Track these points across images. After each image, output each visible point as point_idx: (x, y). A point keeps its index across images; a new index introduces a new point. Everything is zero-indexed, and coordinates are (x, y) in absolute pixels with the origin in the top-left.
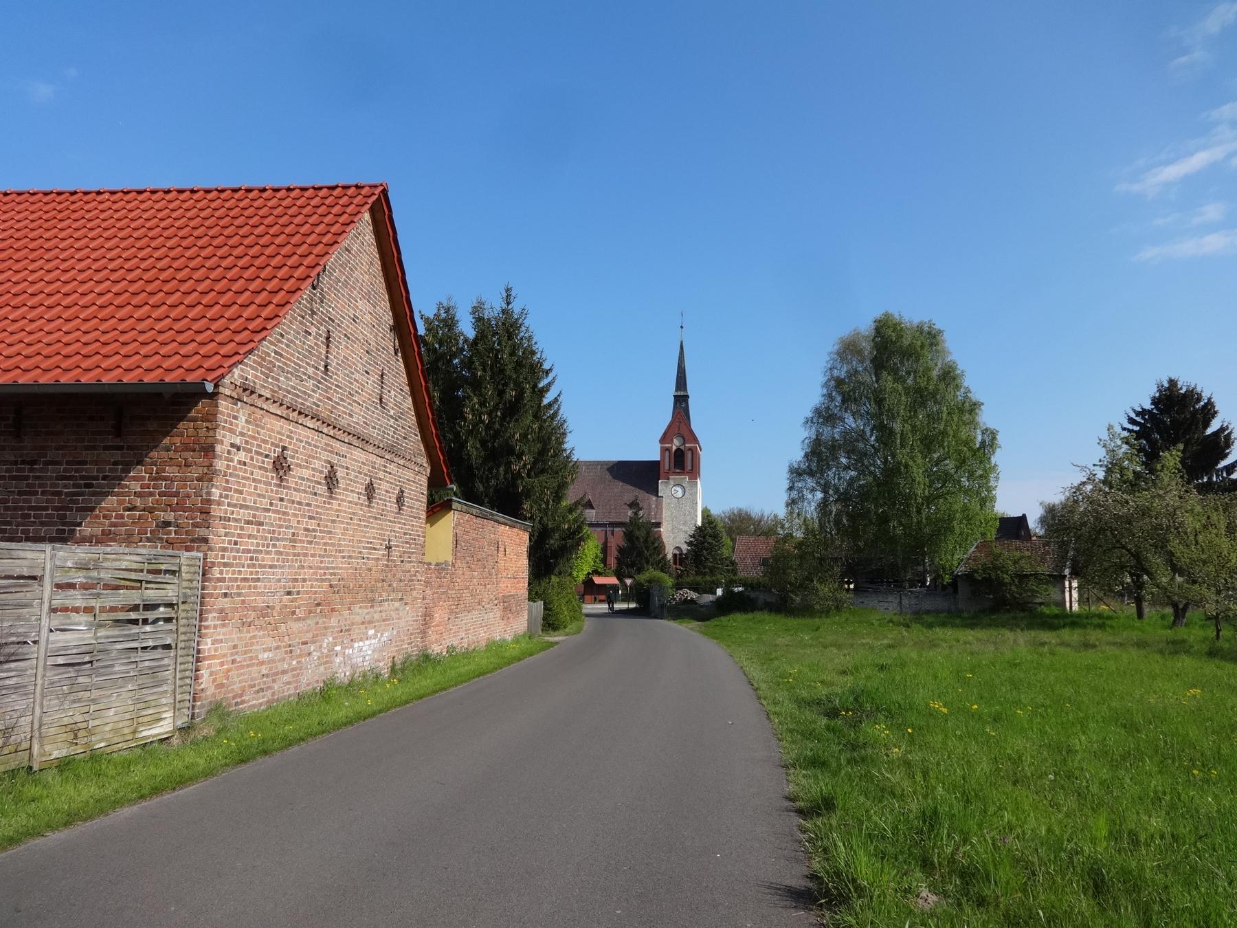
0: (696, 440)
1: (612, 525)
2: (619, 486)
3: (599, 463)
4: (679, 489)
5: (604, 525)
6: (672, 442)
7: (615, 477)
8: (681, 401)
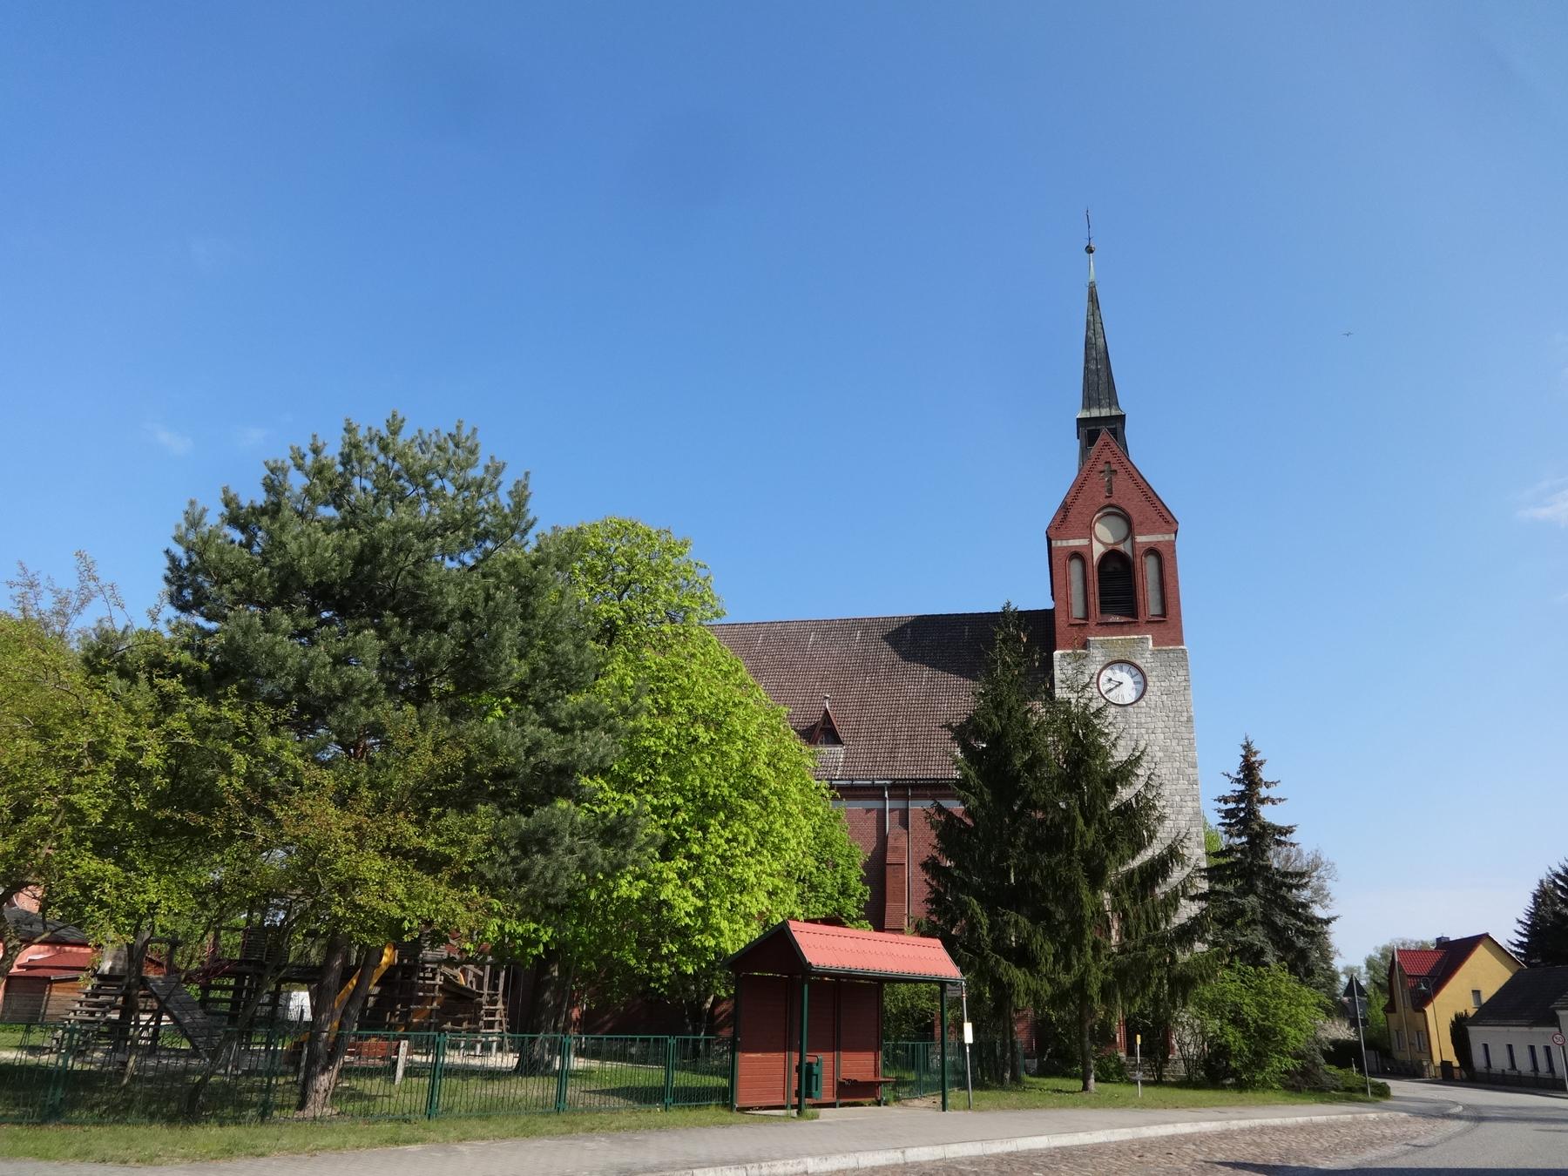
0: (1168, 521)
1: (901, 789)
2: (920, 680)
3: (858, 623)
4: (1123, 675)
5: (873, 792)
6: (1089, 531)
7: (907, 657)
8: (1101, 432)
